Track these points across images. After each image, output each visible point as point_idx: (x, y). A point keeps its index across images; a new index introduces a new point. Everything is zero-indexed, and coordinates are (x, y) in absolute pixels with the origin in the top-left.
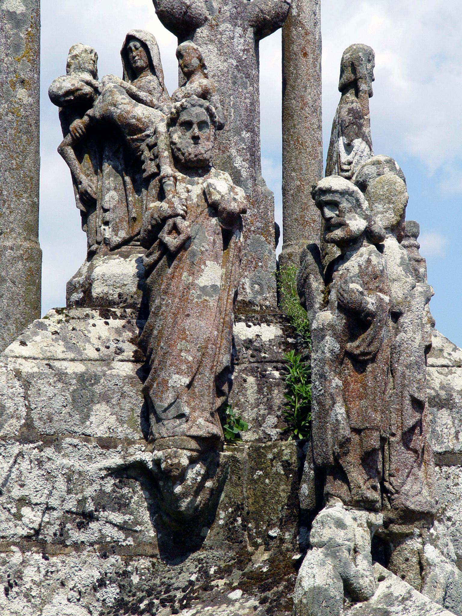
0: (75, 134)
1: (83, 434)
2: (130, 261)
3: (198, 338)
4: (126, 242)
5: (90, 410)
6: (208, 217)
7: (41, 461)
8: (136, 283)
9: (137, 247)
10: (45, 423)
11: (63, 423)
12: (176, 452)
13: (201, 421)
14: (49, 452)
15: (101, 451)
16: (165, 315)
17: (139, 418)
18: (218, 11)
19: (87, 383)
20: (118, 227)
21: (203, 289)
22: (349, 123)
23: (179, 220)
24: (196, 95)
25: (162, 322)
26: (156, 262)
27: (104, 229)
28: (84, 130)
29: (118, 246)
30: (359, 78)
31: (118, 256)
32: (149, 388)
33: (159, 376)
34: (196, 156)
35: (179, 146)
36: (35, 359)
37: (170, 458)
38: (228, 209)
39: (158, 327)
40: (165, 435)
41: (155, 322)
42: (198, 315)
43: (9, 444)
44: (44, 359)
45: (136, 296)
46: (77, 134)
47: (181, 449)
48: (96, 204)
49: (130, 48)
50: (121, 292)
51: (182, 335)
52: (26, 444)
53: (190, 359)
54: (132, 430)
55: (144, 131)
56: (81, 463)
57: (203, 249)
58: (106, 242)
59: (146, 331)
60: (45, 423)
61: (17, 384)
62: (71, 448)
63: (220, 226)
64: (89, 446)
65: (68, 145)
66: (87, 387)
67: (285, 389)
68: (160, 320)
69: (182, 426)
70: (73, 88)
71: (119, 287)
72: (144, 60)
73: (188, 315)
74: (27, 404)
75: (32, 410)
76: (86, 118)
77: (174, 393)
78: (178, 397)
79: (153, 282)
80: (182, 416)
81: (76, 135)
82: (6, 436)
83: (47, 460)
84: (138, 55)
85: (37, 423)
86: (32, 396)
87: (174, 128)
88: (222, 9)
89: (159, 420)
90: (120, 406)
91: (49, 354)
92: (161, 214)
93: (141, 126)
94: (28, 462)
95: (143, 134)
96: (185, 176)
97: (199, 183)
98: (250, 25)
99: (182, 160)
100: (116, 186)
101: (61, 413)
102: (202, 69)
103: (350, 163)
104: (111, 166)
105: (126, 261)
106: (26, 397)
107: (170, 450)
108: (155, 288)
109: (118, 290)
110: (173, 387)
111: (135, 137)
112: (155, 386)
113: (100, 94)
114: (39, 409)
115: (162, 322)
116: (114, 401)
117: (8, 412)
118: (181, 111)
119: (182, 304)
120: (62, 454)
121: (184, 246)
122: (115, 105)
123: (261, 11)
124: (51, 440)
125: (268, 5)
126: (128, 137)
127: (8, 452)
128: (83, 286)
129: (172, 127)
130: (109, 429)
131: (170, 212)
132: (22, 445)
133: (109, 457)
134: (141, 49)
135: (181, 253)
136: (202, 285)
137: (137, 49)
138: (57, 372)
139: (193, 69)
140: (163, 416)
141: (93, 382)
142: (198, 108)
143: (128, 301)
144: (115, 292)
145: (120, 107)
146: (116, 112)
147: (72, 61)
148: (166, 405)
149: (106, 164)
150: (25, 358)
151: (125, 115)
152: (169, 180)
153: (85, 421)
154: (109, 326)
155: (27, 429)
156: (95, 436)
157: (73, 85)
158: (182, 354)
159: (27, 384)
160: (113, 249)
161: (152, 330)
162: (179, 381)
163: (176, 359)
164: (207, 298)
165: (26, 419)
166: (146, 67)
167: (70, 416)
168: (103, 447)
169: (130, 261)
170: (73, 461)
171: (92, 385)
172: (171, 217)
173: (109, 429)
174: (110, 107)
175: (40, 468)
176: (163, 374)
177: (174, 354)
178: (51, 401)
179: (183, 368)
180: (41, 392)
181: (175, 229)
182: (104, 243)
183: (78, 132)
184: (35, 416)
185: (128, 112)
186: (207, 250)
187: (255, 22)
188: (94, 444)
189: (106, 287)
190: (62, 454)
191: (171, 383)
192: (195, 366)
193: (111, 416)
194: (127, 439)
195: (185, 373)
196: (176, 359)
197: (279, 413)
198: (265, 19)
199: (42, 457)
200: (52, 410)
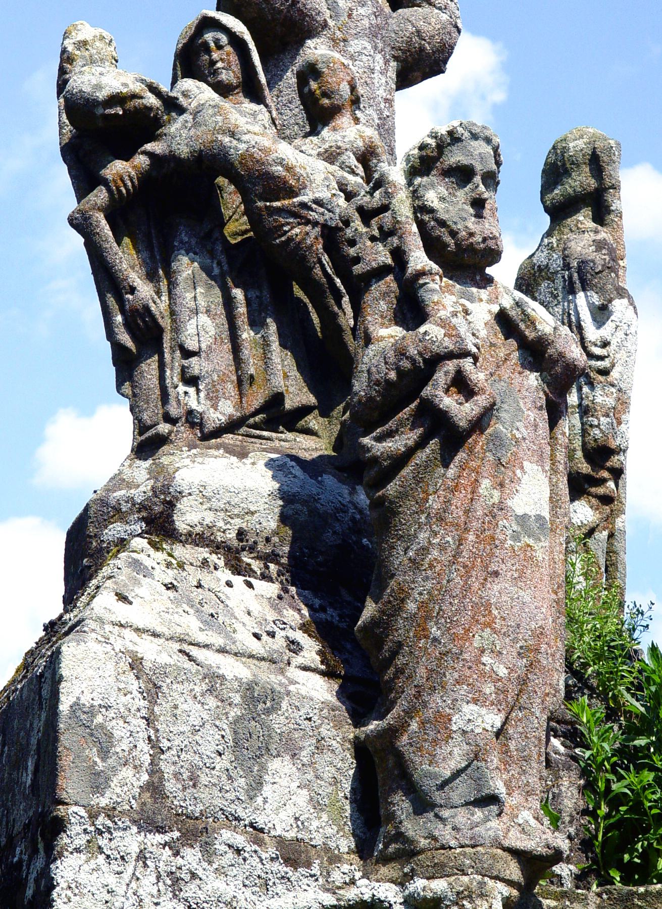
0: (118, 188)
1: (252, 825)
2: (253, 464)
3: (518, 626)
4: (232, 426)
5: (263, 768)
6: (520, 369)
7: (178, 879)
8: (277, 510)
9: (253, 440)
10: (185, 788)
11: (216, 792)
12: (482, 884)
13: (526, 816)
14: (191, 857)
15: (284, 869)
16: (437, 569)
17: (348, 802)
18: (346, 14)
19: (261, 706)
20: (217, 391)
21: (523, 520)
22: (603, 266)
23: (467, 364)
24: (354, 154)
25: (429, 585)
26: (410, 452)
27: (186, 393)
28: (136, 181)
29: (218, 432)
30: (610, 188)
31: (221, 451)
32: (397, 731)
33: (425, 705)
34: (485, 240)
35: (442, 215)
36: (155, 635)
37: (470, 897)
38: (567, 355)
39: (420, 594)
40: (453, 843)
41: (413, 582)
42: (516, 575)
43: (119, 828)
44: (172, 638)
45: (275, 539)
46: (124, 191)
47: (491, 878)
48: (162, 339)
49: (206, 45)
50: (244, 525)
51: (484, 616)
52: (150, 831)
53: (502, 671)
54: (335, 828)
55: (297, 195)
56: (248, 892)
57: (518, 435)
58: (192, 419)
59: (390, 602)
60: (185, 788)
61: (134, 685)
62: (230, 855)
63: (545, 392)
64: (264, 856)
65: (99, 210)
66: (259, 715)
67: (580, 778)
68: (426, 579)
69: (489, 824)
70: (125, 91)
71: (238, 516)
72: (234, 72)
73: (496, 574)
74: (153, 737)
75: (163, 752)
76: (141, 160)
77: (466, 747)
78: (476, 757)
79: (403, 495)
80: (490, 800)
81: (119, 191)
82: (114, 808)
83: (187, 877)
84: (221, 59)
85: (171, 786)
86: (162, 718)
87: (425, 179)
88: (355, 12)
89: (423, 805)
90: (316, 770)
91: (179, 630)
92: (426, 348)
93: (292, 182)
94: (153, 879)
95: (295, 200)
96: (451, 282)
97: (481, 300)
98: (394, 57)
99: (448, 246)
100: (209, 306)
101: (214, 768)
102: (353, 107)
103: (605, 344)
104: (196, 264)
105: (244, 464)
106: (149, 721)
107: (465, 879)
108: (408, 508)
109: (237, 523)
110: (464, 732)
111: (277, 204)
112: (414, 726)
113: (181, 110)
114: (174, 752)
115: (429, 585)
116: (305, 756)
117: (118, 750)
118: (449, 145)
119: (481, 547)
120: (215, 866)
121: (479, 424)
122: (233, 135)
123: (418, 32)
124: (194, 831)
125: (430, 24)
126: (260, 204)
127: (116, 848)
128: (143, 507)
129: (422, 176)
130: (297, 819)
131: (449, 344)
132: (143, 834)
133: (297, 888)
134: (229, 49)
135: (474, 437)
136: (520, 512)
137: (220, 47)
138: (206, 671)
139: (340, 103)
140: (438, 797)
141: (268, 704)
142: (482, 143)
143: (260, 547)
144: (228, 526)
145: (245, 138)
146: (236, 149)
147: (77, 52)
148: (448, 774)
149: (185, 260)
150: (137, 630)
151: (258, 155)
152: (433, 280)
153: (255, 796)
154: (255, 592)
155: (151, 796)
156: (273, 833)
157: (125, 85)
158: (484, 659)
159: (153, 691)
160: (206, 437)
161: (403, 601)
162: (480, 720)
163: (470, 668)
164: (531, 542)
165: (151, 773)
166: (237, 87)
167: (230, 778)
168: (288, 861)
169: (253, 464)
170: (233, 888)
171: (268, 712)
172: (451, 356)
173: (297, 819)
174: (220, 137)
175: (175, 896)
176: (436, 701)
177: (466, 656)
178: (197, 738)
179: (488, 691)
180: (178, 712)
181: (462, 385)
182: (187, 421)
183: (125, 185)
184: (168, 769)
185: (266, 151)
186: (524, 439)
187: (404, 52)
188: (272, 851)
189: (208, 513)
190: (215, 866)
191: (458, 722)
192: (513, 690)
193: (299, 790)
194: (327, 849)
195: (492, 704)
196: (470, 668)
197: (572, 830)
198: (422, 49)
199: (180, 868)
200: (197, 758)
